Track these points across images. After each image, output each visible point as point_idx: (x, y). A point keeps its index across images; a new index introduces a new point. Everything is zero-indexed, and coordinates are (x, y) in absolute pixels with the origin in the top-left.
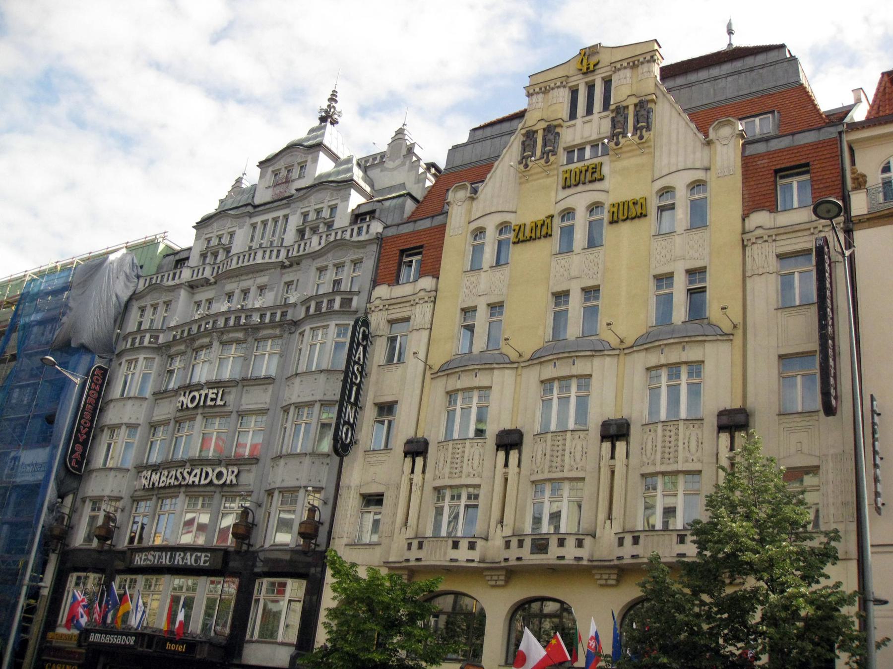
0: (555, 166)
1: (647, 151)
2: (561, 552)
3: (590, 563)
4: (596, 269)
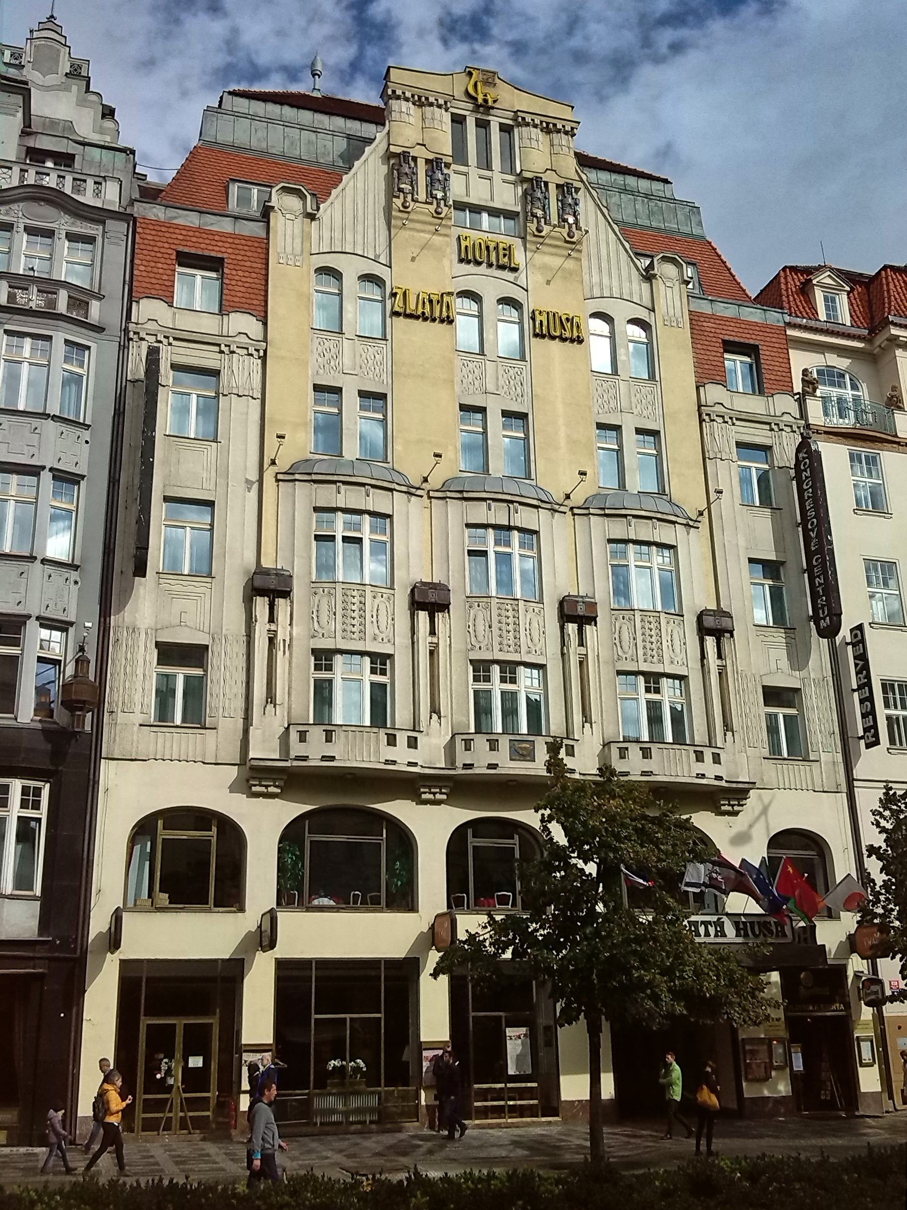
1: (442, 230)
3: (582, 777)
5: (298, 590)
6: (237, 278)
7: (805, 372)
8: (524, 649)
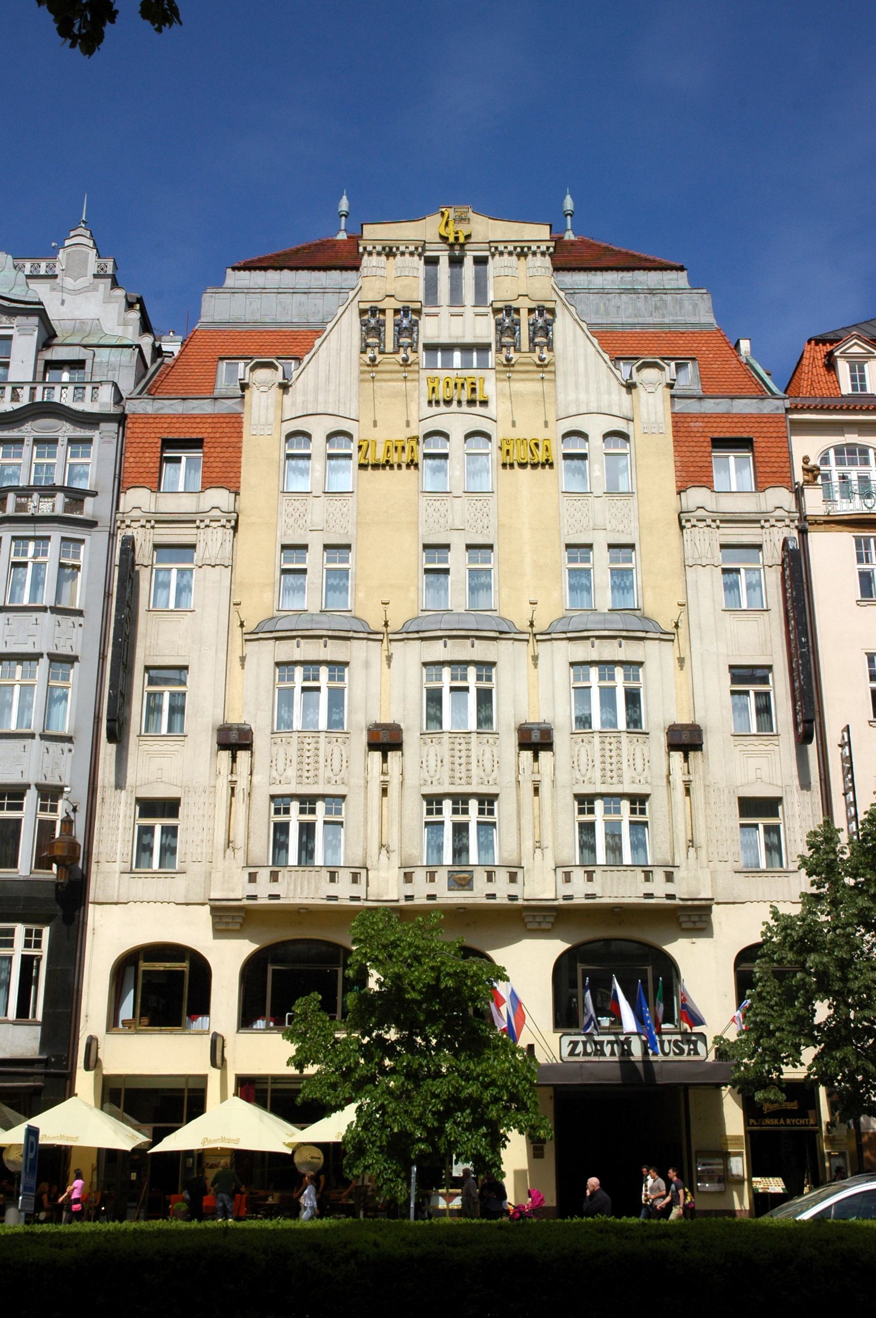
0: (416, 368)
1: (410, 376)
2: (490, 888)
3: (526, 903)
4: (486, 521)
5: (260, 742)
6: (215, 455)
7: (806, 460)
8: (475, 780)
